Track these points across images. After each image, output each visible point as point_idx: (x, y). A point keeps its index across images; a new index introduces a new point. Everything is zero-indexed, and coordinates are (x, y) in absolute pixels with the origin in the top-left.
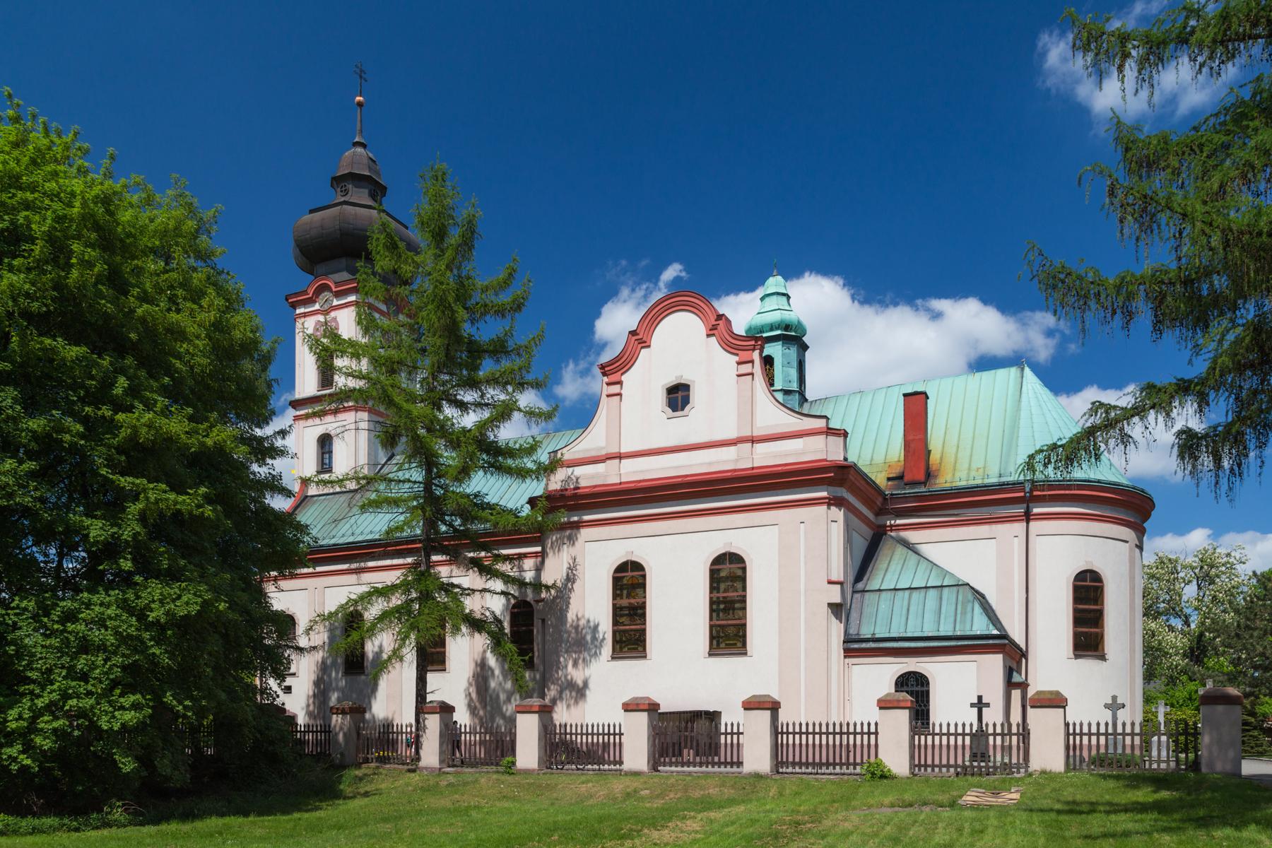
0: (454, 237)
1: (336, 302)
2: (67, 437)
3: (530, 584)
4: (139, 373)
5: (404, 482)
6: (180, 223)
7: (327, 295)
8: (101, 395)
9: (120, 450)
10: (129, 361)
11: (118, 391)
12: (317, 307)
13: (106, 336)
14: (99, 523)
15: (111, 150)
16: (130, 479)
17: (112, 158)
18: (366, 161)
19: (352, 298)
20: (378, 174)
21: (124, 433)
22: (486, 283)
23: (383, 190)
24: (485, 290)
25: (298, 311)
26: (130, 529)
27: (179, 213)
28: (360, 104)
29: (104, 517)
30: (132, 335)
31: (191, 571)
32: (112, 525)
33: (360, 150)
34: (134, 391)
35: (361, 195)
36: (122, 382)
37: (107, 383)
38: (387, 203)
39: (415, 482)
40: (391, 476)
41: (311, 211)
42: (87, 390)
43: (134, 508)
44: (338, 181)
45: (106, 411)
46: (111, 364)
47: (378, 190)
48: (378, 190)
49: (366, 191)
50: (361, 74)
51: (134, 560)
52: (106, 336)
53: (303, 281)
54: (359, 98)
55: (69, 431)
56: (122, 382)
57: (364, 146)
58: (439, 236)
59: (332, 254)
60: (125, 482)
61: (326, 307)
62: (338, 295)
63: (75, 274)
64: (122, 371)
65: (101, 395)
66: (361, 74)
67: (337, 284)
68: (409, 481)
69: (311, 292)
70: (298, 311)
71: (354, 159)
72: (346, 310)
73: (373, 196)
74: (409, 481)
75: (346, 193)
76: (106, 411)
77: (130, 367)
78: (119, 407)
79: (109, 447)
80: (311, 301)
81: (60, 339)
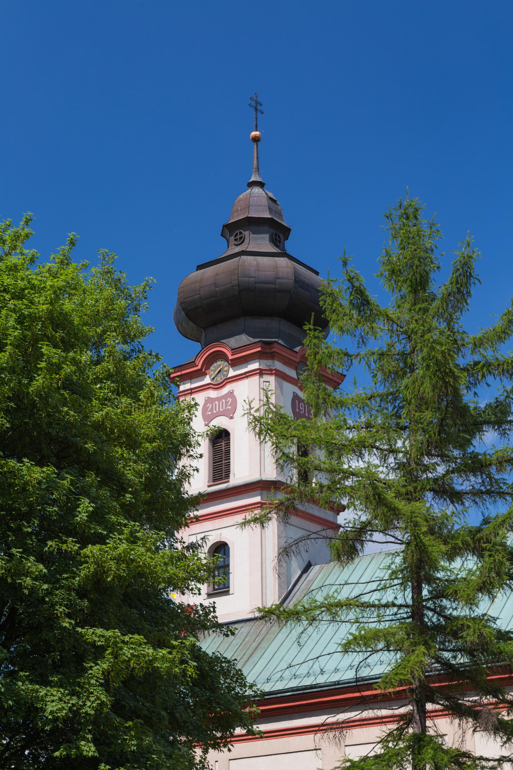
0: (440, 284)
1: (232, 373)
2: (29, 581)
3: (424, 728)
4: (101, 492)
5: (386, 606)
6: (111, 301)
7: (220, 364)
8: (63, 525)
9: (82, 593)
10: (91, 478)
11: (82, 516)
12: (207, 380)
13: (62, 450)
14: (56, 693)
15: (71, 235)
16: (99, 631)
17: (72, 243)
18: (265, 201)
19: (255, 366)
20: (279, 214)
21: (85, 571)
22: (479, 335)
23: (286, 231)
24: (477, 345)
25: (182, 388)
26: (95, 699)
27: (109, 291)
28: (256, 140)
29: (60, 685)
30: (88, 446)
31: (158, 753)
32: (73, 693)
33: (257, 190)
34: (97, 516)
35: (261, 242)
36: (85, 507)
37: (70, 509)
38: (289, 245)
39: (400, 606)
40: (365, 599)
41: (200, 267)
42: (44, 518)
43: (97, 669)
44: (234, 230)
45: (71, 545)
46: (72, 483)
47: (278, 232)
48: (278, 232)
49: (267, 236)
50: (256, 106)
51: (95, 741)
52: (62, 450)
53: (190, 350)
54: (254, 133)
55: (28, 574)
56: (85, 507)
57: (261, 185)
58: (419, 284)
59: (262, 315)
60: (94, 634)
61: (219, 379)
62: (235, 363)
63: (39, 381)
64: (84, 492)
65: (63, 525)
66: (256, 106)
67: (234, 351)
68: (394, 605)
69: (200, 364)
70: (182, 388)
71: (255, 202)
72: (246, 381)
73: (275, 241)
74: (394, 605)
75: (241, 240)
76: (71, 545)
77: (91, 486)
78: (85, 541)
79: (69, 589)
80: (200, 374)
81: (25, 460)
